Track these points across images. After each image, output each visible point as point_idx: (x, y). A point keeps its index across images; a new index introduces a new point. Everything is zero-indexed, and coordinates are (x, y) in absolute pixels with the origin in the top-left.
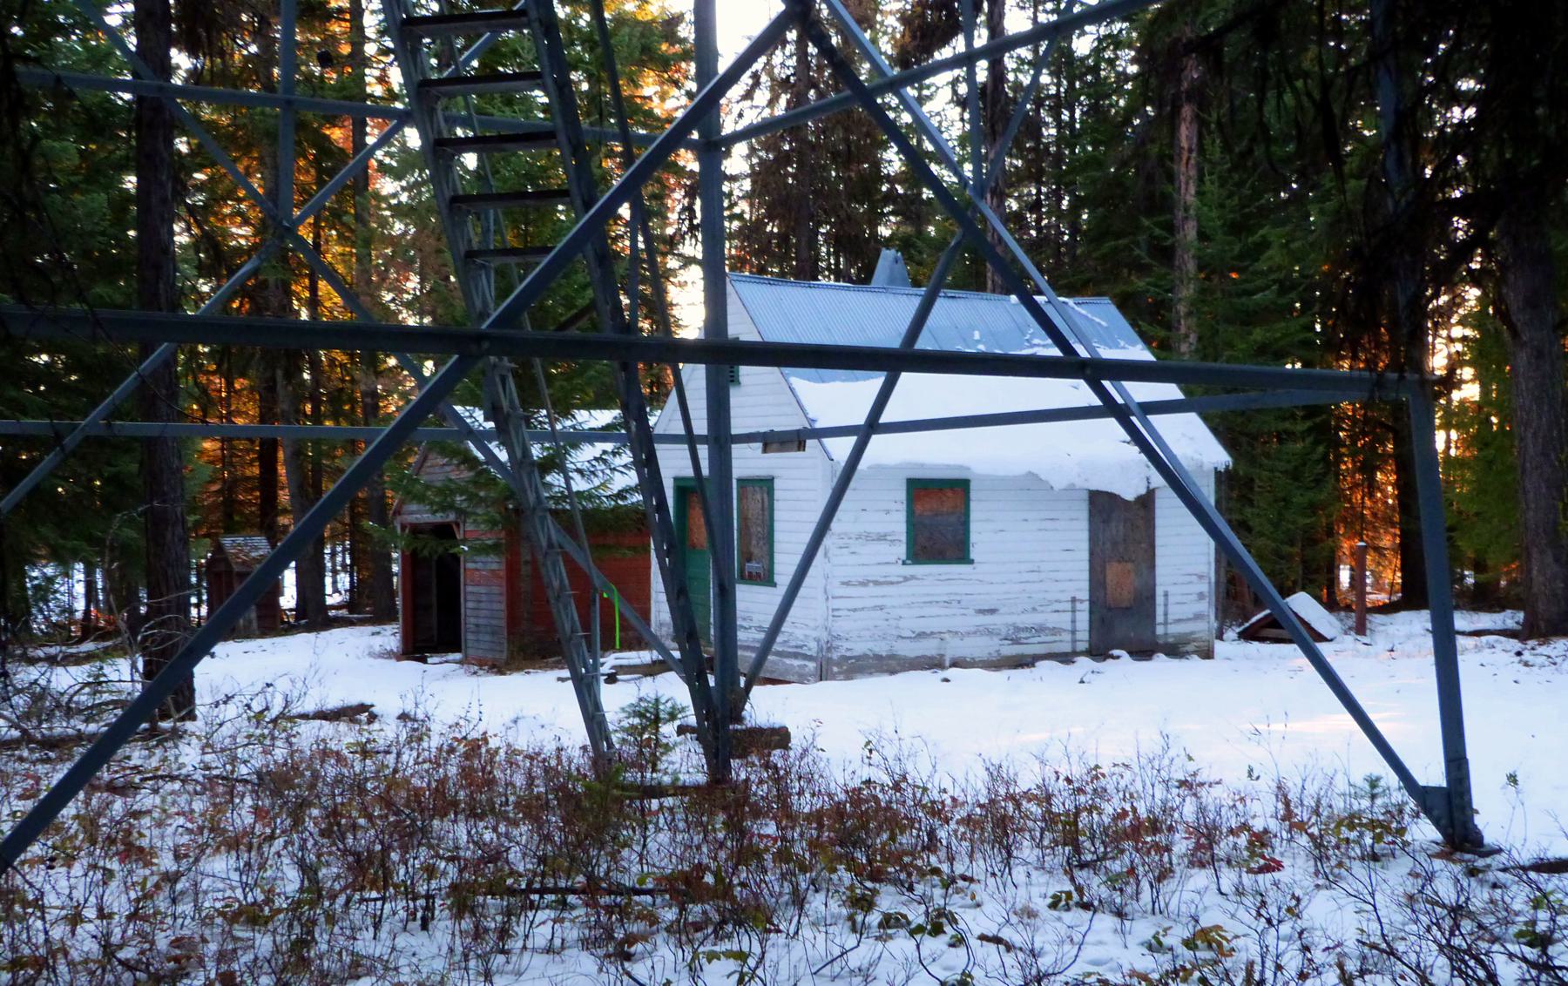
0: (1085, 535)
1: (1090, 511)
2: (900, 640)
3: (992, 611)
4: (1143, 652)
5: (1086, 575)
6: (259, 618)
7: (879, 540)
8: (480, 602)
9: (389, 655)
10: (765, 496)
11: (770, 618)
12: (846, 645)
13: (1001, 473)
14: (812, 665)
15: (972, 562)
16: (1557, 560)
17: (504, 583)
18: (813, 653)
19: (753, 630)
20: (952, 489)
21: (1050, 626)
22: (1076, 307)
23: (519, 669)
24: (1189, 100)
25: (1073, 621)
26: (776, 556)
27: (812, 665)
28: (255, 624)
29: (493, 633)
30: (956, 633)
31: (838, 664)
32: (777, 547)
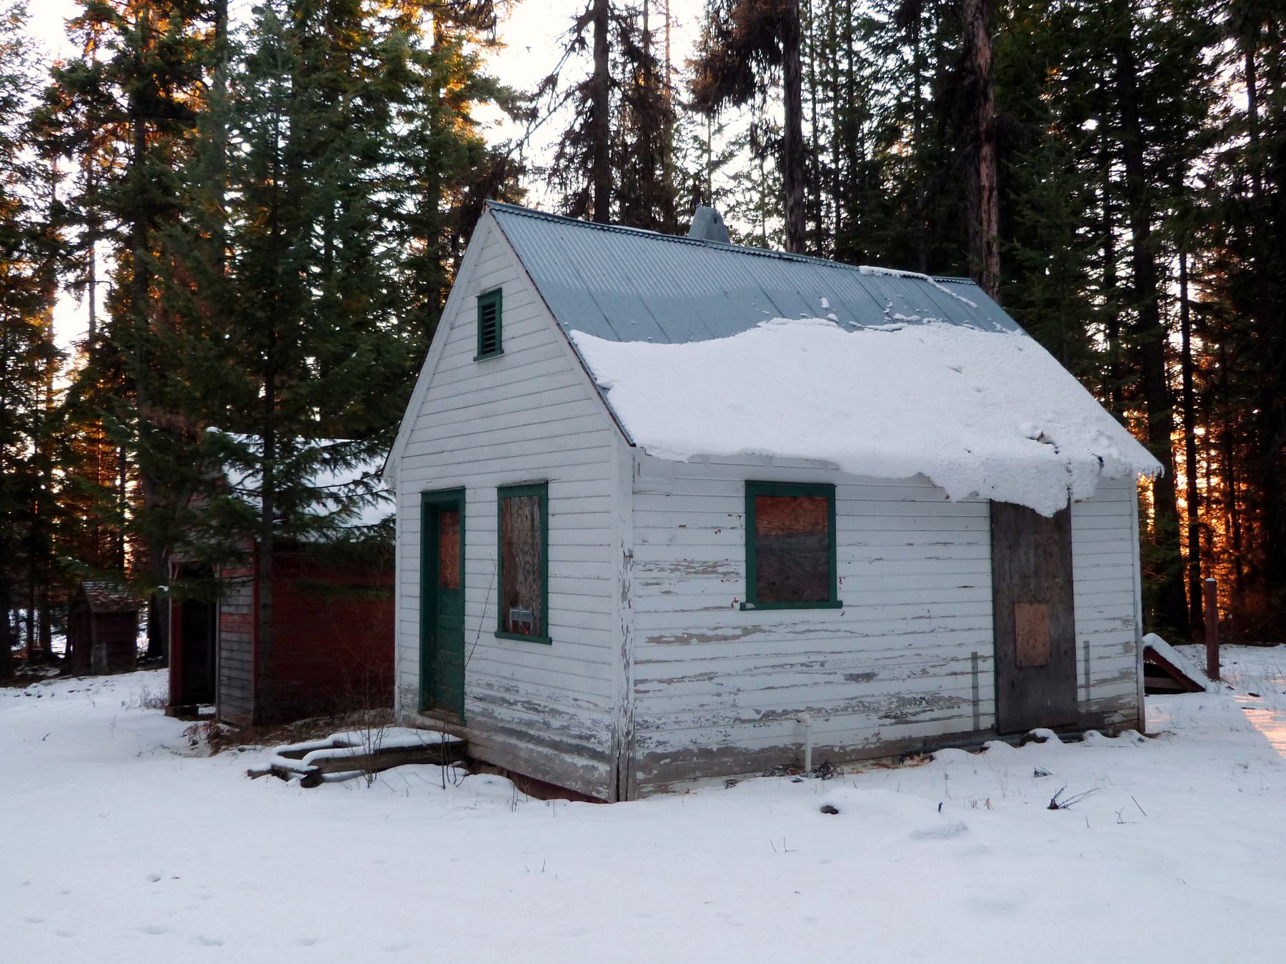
0: (986, 566)
1: (992, 531)
2: (738, 726)
3: (868, 677)
4: (1071, 730)
5: (989, 622)
6: (109, 655)
7: (704, 572)
8: (232, 651)
10: (536, 508)
12: (657, 736)
13: (883, 473)
14: (603, 768)
15: (839, 605)
18: (606, 748)
19: (519, 706)
20: (812, 500)
21: (946, 694)
22: (938, 285)
24: (988, 140)
25: (975, 687)
26: (551, 597)
27: (603, 768)
28: (105, 662)
29: (243, 688)
30: (819, 710)
31: (645, 767)
32: (552, 582)
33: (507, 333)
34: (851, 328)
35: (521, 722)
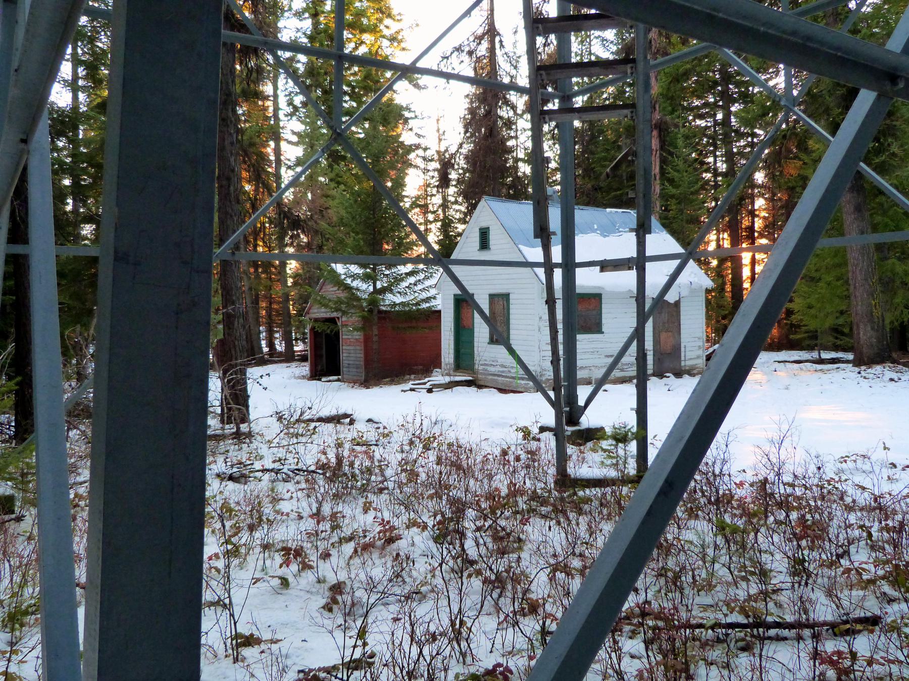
9: (304, 377)
11: (754, 376)
15: (603, 333)
16: (872, 329)
17: (363, 345)
23: (376, 385)
29: (357, 368)
32: (511, 326)
33: (491, 242)
34: (605, 236)
35: (499, 371)
